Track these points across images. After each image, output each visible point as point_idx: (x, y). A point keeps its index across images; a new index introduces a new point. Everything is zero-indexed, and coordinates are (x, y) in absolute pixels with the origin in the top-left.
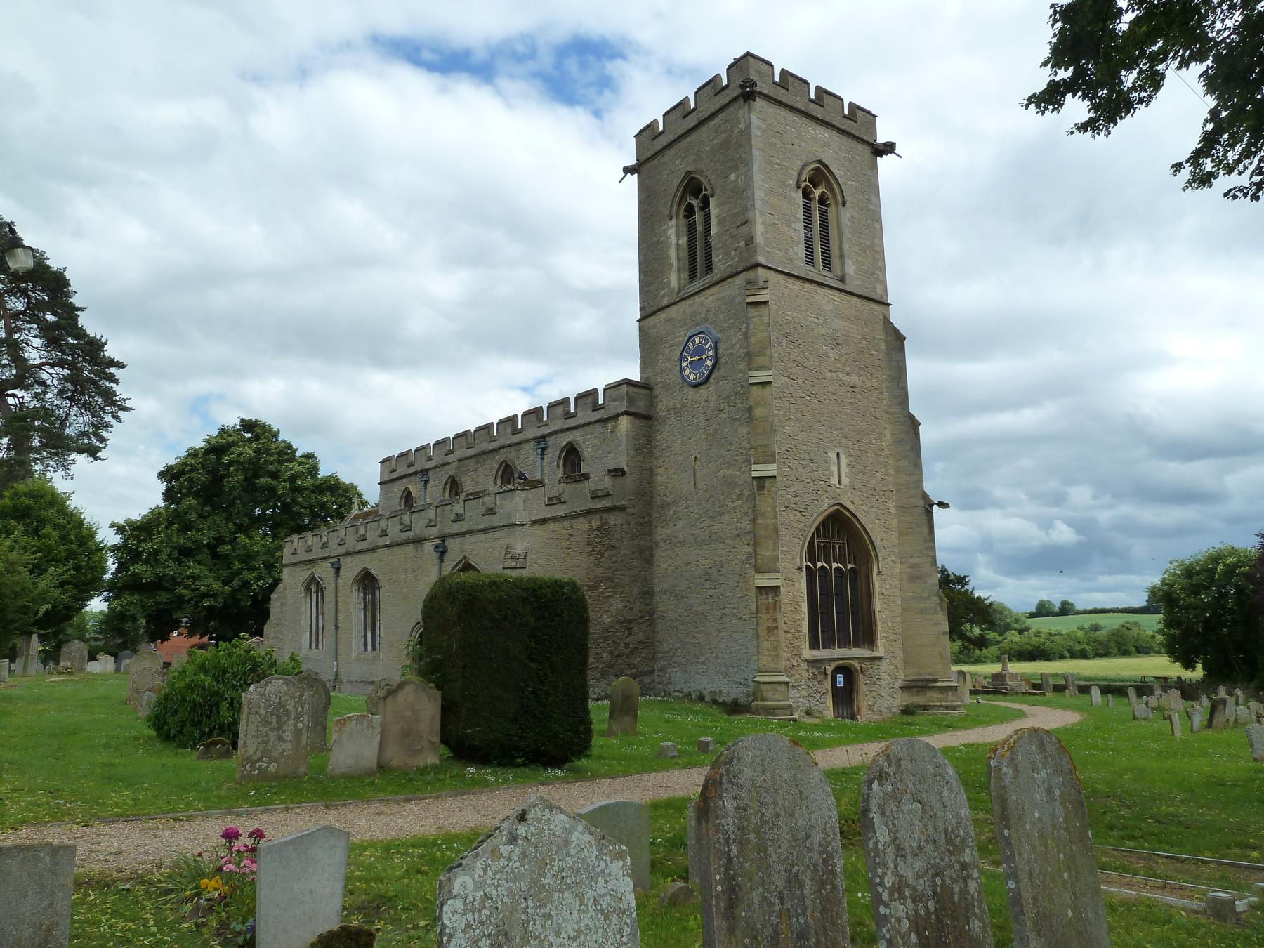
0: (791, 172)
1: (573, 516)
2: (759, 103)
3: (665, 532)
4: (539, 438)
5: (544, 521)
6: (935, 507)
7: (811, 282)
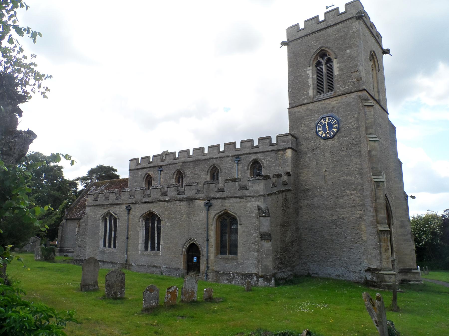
3: (306, 202)
6: (409, 198)
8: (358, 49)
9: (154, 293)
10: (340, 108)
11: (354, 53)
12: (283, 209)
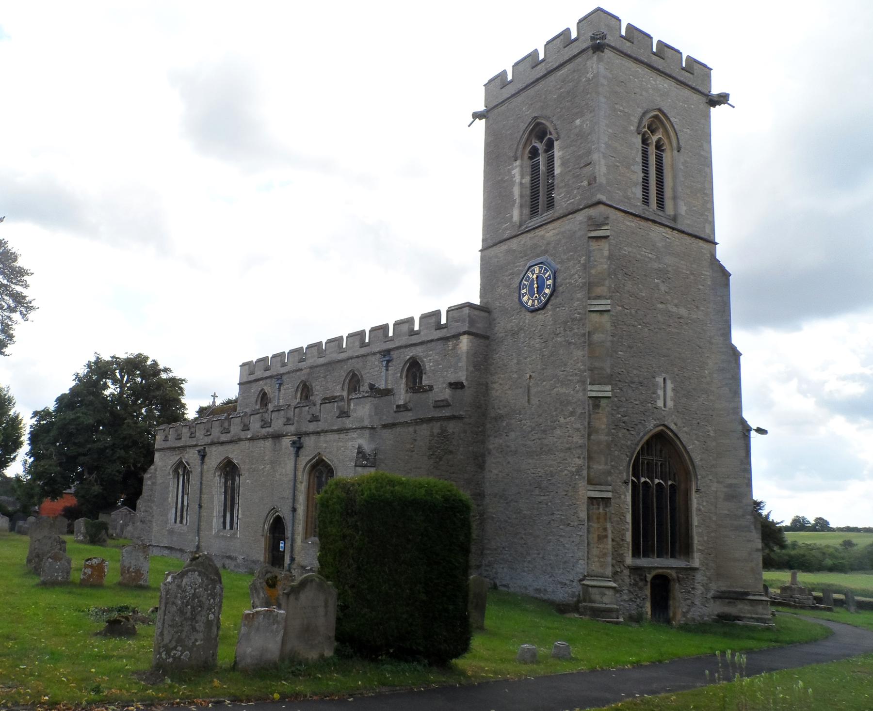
0: (632, 118)
1: (424, 421)
2: (608, 53)
4: (385, 351)
5: (393, 425)
6: (753, 434)
7: (647, 220)
8: (593, 116)
9: (61, 563)
10: (558, 244)
11: (587, 125)
12: (431, 453)
